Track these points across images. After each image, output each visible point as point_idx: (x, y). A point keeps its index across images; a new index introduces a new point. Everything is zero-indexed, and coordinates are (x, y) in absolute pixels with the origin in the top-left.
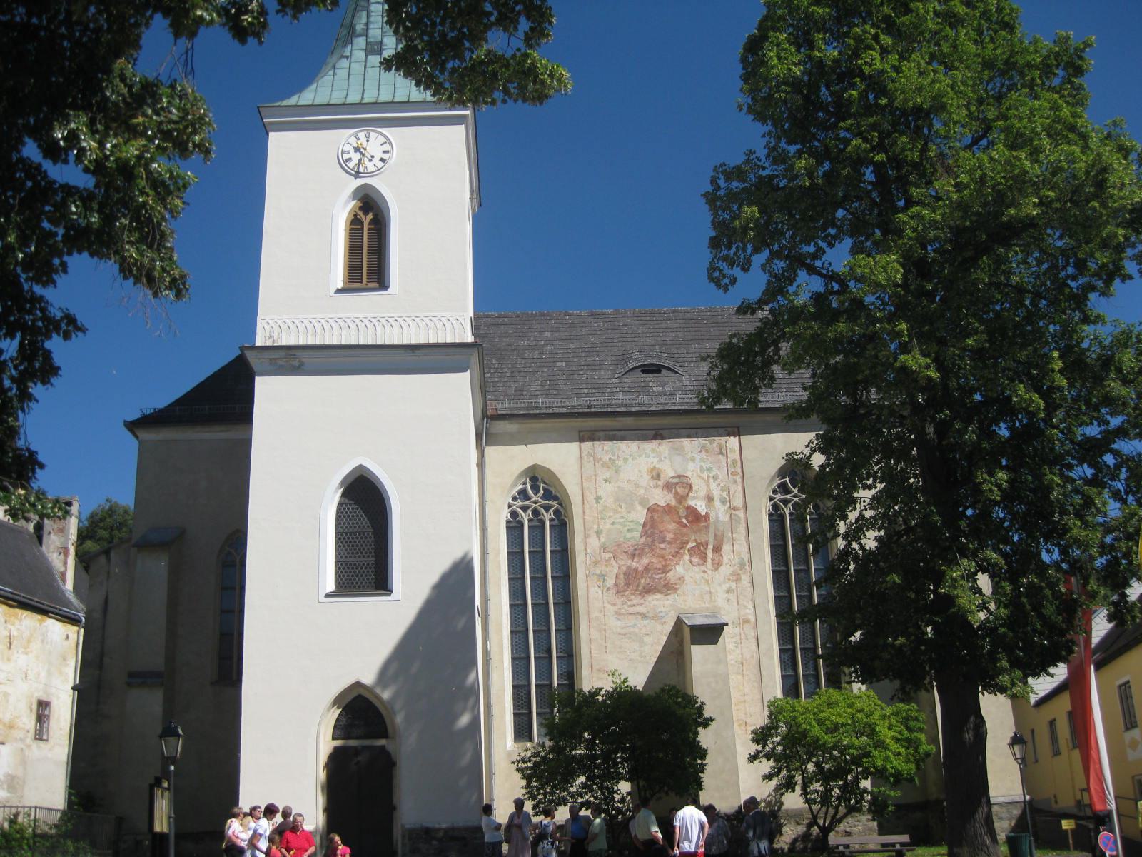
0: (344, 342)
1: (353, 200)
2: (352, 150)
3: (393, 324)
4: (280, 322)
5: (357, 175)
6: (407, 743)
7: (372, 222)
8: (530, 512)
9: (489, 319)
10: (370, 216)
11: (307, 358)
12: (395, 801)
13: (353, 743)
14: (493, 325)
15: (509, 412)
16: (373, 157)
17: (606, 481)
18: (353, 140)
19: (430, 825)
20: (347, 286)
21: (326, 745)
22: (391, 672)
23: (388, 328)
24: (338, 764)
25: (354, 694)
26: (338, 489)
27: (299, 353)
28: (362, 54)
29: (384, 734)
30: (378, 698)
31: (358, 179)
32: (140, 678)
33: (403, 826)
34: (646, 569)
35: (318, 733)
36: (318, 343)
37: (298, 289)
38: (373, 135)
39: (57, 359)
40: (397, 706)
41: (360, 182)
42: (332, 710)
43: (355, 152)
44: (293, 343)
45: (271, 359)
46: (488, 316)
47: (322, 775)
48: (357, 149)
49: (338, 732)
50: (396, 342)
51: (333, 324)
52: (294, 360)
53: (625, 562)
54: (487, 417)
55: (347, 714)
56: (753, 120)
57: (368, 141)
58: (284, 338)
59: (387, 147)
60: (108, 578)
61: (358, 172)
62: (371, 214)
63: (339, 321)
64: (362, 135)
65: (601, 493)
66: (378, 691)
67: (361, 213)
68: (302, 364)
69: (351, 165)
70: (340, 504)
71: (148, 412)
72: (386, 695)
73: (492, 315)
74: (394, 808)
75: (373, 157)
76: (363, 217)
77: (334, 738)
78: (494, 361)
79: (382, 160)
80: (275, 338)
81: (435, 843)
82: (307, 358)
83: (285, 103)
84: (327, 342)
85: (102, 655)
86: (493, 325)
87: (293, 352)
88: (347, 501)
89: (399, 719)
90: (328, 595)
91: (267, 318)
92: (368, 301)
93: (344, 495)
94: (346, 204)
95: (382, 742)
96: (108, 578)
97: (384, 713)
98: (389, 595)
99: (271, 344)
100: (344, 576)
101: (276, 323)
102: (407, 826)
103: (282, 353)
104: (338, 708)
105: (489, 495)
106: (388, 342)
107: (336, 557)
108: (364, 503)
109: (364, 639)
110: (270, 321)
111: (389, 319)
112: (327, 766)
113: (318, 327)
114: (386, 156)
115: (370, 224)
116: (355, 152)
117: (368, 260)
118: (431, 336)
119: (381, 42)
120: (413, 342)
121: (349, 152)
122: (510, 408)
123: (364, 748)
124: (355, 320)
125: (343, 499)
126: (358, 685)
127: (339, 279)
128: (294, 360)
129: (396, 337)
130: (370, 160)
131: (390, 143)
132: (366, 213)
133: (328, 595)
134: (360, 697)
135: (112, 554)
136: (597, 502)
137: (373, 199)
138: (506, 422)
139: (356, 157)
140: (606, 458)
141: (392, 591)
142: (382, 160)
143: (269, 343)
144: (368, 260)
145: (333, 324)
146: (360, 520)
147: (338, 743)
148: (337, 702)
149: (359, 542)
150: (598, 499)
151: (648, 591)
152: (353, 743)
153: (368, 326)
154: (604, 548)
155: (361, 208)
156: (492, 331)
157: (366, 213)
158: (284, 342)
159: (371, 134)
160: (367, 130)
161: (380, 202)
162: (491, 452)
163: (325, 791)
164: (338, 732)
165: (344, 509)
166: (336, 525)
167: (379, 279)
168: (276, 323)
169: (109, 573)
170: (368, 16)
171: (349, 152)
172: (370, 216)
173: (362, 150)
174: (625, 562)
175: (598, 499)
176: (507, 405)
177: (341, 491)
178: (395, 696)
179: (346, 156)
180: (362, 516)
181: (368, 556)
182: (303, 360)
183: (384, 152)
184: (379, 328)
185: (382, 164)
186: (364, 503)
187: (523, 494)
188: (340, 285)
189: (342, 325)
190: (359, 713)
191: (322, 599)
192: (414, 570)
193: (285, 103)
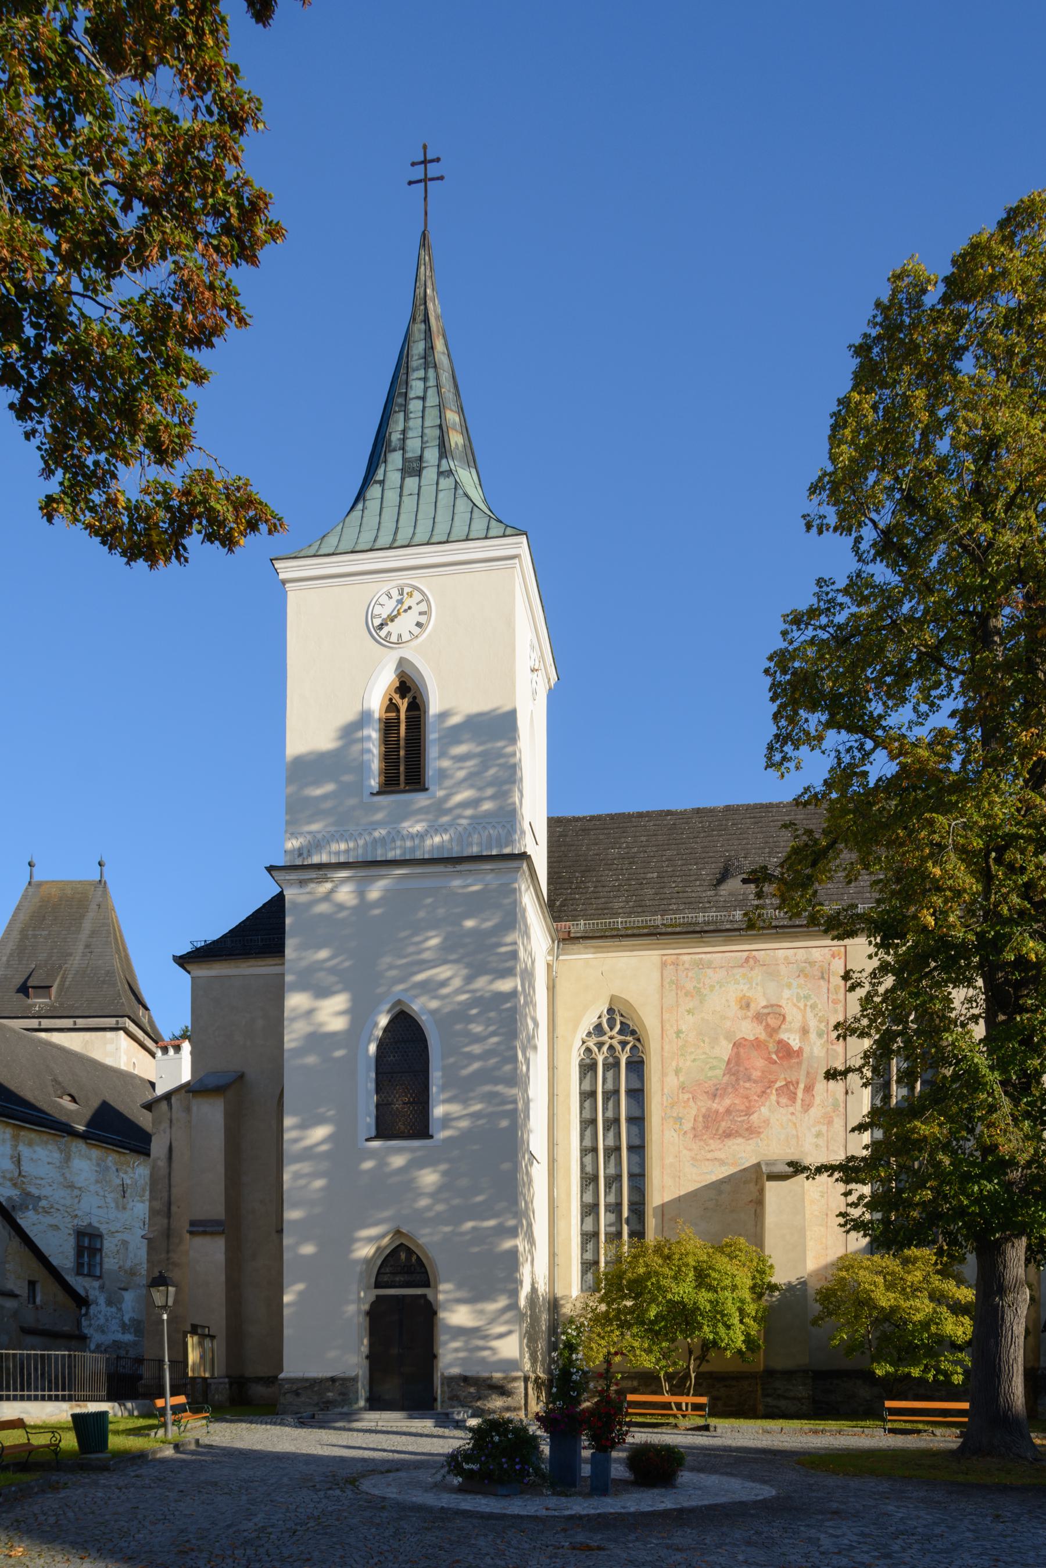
8: (605, 1048)
17: (689, 1012)
28: (398, 476)
34: (728, 1111)
53: (706, 1104)
65: (684, 1028)
67: (397, 698)
74: (435, 1356)
85: (169, 1204)
114: (423, 619)
119: (421, 457)
127: (374, 783)
131: (428, 601)
135: (173, 1100)
136: (678, 1037)
140: (689, 986)
150: (678, 1033)
151: (728, 1135)
154: (683, 1088)
169: (171, 1121)
170: (406, 419)
174: (706, 1104)
175: (678, 1033)
187: (598, 1029)
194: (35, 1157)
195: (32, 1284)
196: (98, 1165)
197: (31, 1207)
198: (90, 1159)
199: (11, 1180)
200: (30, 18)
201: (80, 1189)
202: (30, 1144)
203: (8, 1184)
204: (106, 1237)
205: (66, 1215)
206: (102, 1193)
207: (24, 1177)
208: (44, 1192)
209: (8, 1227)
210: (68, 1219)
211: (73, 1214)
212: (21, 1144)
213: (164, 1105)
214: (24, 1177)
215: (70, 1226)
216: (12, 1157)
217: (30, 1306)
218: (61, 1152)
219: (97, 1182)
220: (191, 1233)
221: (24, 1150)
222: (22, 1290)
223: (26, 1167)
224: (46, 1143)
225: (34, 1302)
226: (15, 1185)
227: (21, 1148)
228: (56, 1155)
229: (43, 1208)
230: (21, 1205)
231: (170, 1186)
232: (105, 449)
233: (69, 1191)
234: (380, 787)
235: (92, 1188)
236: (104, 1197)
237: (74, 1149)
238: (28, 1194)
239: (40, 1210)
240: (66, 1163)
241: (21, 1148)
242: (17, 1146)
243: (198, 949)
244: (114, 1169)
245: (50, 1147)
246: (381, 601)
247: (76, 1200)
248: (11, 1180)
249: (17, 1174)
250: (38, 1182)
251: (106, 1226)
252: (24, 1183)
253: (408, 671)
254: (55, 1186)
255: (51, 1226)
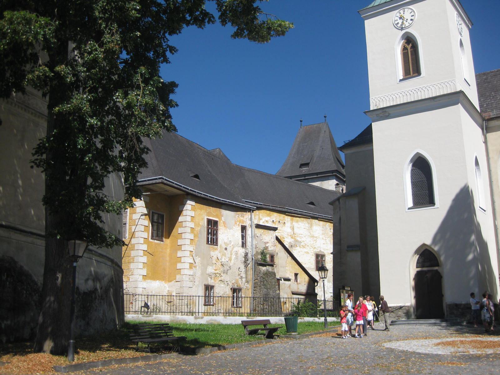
0: (405, 102)
1: (402, 40)
2: (399, 19)
3: (432, 88)
4: (379, 99)
5: (402, 29)
6: (447, 268)
7: (411, 48)
9: (492, 74)
10: (410, 45)
11: (391, 111)
12: (443, 293)
13: (425, 269)
14: (494, 76)
15: (496, 116)
16: (407, 19)
18: (398, 15)
19: (457, 303)
20: (405, 77)
21: (413, 270)
22: (438, 238)
23: (422, 91)
24: (419, 278)
25: (424, 248)
26: (409, 164)
27: (387, 110)
29: (438, 265)
30: (433, 249)
31: (403, 31)
32: (352, 248)
33: (446, 303)
35: (409, 267)
36: (395, 104)
37: (385, 82)
38: (406, 10)
39: (146, 160)
40: (442, 252)
41: (404, 32)
42: (415, 256)
43: (400, 19)
44: (385, 106)
45: (377, 115)
46: (492, 72)
47: (413, 283)
48: (400, 18)
49: (418, 265)
50: (427, 97)
51: (397, 96)
52: (386, 113)
54: (485, 120)
55: (422, 257)
56: (237, 35)
57: (404, 13)
58: (381, 105)
59: (413, 14)
60: (340, 210)
61: (402, 28)
62: (410, 44)
63: (435, 86)
64: (402, 12)
66: (433, 247)
67: (406, 45)
68: (389, 114)
69: (399, 25)
70: (412, 170)
71: (347, 142)
72: (436, 248)
73: (494, 71)
74: (443, 296)
75: (407, 19)
76: (408, 46)
77: (417, 267)
78: (493, 93)
79: (411, 20)
80: (378, 105)
81: (460, 310)
82: (391, 111)
83: (369, 7)
84: (398, 103)
85: (340, 240)
86: (494, 76)
87: (384, 110)
88: (414, 168)
89: (442, 258)
90: (409, 209)
91: (374, 98)
92: (414, 82)
93: (413, 166)
94: (399, 43)
95: (436, 268)
96: (340, 210)
97: (436, 256)
98: (434, 206)
99: (376, 108)
100: (416, 200)
101: (378, 99)
102: (448, 303)
103: (380, 111)
104: (418, 255)
105: (491, 155)
106: (423, 98)
107: (412, 192)
108: (421, 167)
109: (425, 226)
110: (375, 99)
111: (423, 88)
112: (414, 279)
113: (394, 97)
114: (413, 18)
115: (411, 49)
116: (400, 19)
117: (412, 65)
118: (441, 92)
120: (434, 96)
121: (397, 20)
122: (497, 114)
123: (429, 271)
124: (409, 91)
125: (413, 167)
126: (424, 245)
128: (386, 113)
129: (426, 95)
130: (407, 21)
131: (414, 11)
132: (408, 44)
133: (409, 209)
134: (426, 250)
135: (340, 200)
137: (410, 38)
138: (496, 121)
139: (400, 21)
141: (435, 204)
142: (411, 20)
143: (375, 108)
144: (412, 65)
145: (397, 96)
146: (420, 175)
147: (419, 269)
148: (416, 252)
149: (421, 185)
152: (425, 269)
153: (414, 93)
155: (406, 43)
156: (493, 79)
157: (408, 44)
158: (382, 107)
159: (405, 9)
160: (404, 9)
161: (413, 38)
162: (489, 135)
163: (414, 289)
164: (418, 265)
165: (414, 172)
166: (411, 179)
167: (417, 72)
168: (378, 99)
169: (340, 208)
171: (397, 20)
172: (410, 45)
173: (402, 18)
176: (495, 113)
177: (411, 165)
178: (440, 249)
179: (396, 22)
180: (421, 174)
181: (425, 190)
182: (390, 112)
183: (412, 16)
184: (419, 93)
185: (412, 21)
186: (421, 167)
188: (401, 78)
189: (404, 94)
190: (426, 256)
191: (407, 210)
192: (444, 195)
193: (369, 7)
194: (299, 226)
195: (296, 275)
196: (323, 227)
197: (298, 245)
198: (320, 226)
199: (291, 236)
200: (107, 65)
201: (316, 237)
202: (297, 222)
203: (290, 237)
204: (326, 255)
205: (311, 247)
206: (325, 238)
207: (295, 234)
208: (303, 239)
209: (287, 253)
210: (312, 249)
211: (314, 247)
212: (294, 222)
213: (337, 203)
214: (295, 234)
215: (313, 252)
216: (291, 227)
217: (296, 283)
218: (309, 224)
219: (323, 234)
220: (347, 251)
221: (295, 224)
222: (292, 277)
223: (296, 230)
224: (303, 221)
225: (297, 281)
226: (292, 237)
227: (294, 223)
228: (307, 225)
229: (303, 245)
230: (294, 245)
231: (340, 233)
232: (44, 153)
233: (312, 238)
234: (403, 76)
235: (321, 237)
236: (326, 240)
237: (313, 222)
238: (297, 241)
239: (301, 246)
240: (311, 227)
241: (294, 223)
242: (292, 223)
243: (346, 144)
244: (329, 229)
245: (304, 222)
246: (396, 19)
247: (315, 242)
248: (291, 236)
249: (292, 233)
250: (300, 236)
251: (327, 251)
252: (295, 236)
253: (410, 36)
254: (307, 237)
255: (306, 252)
